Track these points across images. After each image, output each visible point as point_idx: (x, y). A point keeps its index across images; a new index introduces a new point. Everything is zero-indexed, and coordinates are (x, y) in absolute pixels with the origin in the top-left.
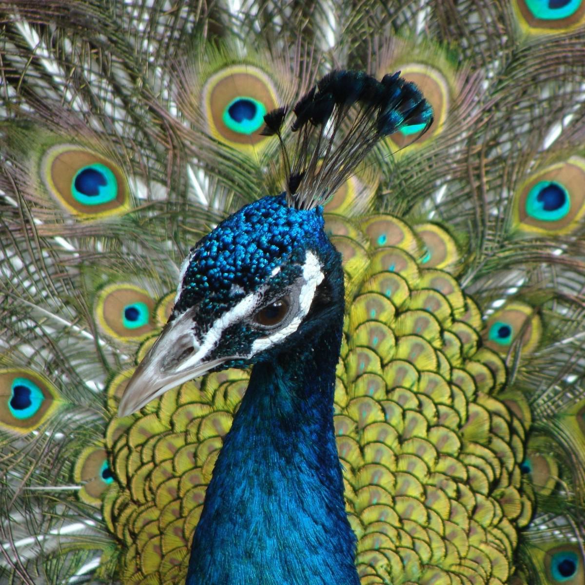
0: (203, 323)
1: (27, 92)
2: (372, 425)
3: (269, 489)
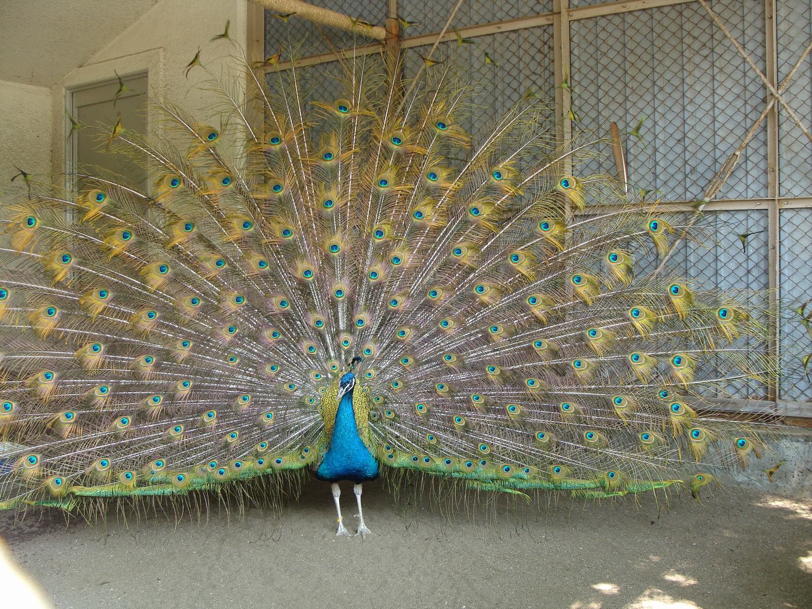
0: (344, 388)
1: (309, 366)
2: (789, 210)
3: (346, 407)
